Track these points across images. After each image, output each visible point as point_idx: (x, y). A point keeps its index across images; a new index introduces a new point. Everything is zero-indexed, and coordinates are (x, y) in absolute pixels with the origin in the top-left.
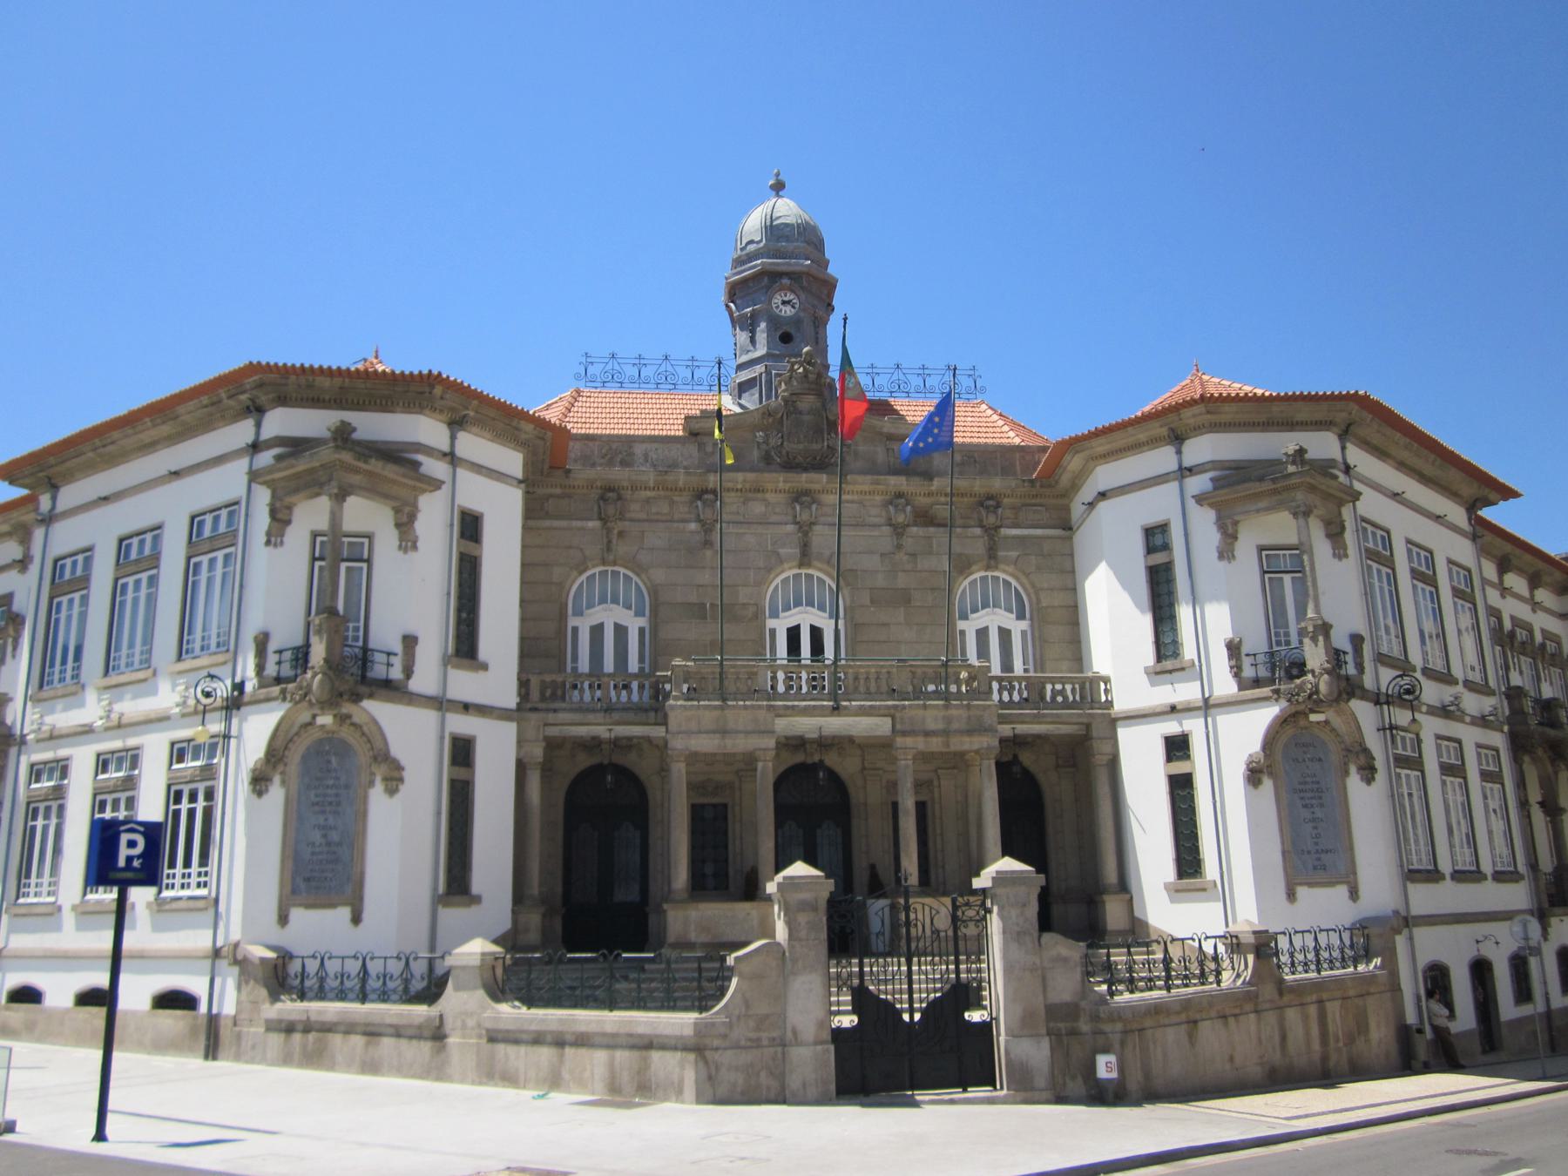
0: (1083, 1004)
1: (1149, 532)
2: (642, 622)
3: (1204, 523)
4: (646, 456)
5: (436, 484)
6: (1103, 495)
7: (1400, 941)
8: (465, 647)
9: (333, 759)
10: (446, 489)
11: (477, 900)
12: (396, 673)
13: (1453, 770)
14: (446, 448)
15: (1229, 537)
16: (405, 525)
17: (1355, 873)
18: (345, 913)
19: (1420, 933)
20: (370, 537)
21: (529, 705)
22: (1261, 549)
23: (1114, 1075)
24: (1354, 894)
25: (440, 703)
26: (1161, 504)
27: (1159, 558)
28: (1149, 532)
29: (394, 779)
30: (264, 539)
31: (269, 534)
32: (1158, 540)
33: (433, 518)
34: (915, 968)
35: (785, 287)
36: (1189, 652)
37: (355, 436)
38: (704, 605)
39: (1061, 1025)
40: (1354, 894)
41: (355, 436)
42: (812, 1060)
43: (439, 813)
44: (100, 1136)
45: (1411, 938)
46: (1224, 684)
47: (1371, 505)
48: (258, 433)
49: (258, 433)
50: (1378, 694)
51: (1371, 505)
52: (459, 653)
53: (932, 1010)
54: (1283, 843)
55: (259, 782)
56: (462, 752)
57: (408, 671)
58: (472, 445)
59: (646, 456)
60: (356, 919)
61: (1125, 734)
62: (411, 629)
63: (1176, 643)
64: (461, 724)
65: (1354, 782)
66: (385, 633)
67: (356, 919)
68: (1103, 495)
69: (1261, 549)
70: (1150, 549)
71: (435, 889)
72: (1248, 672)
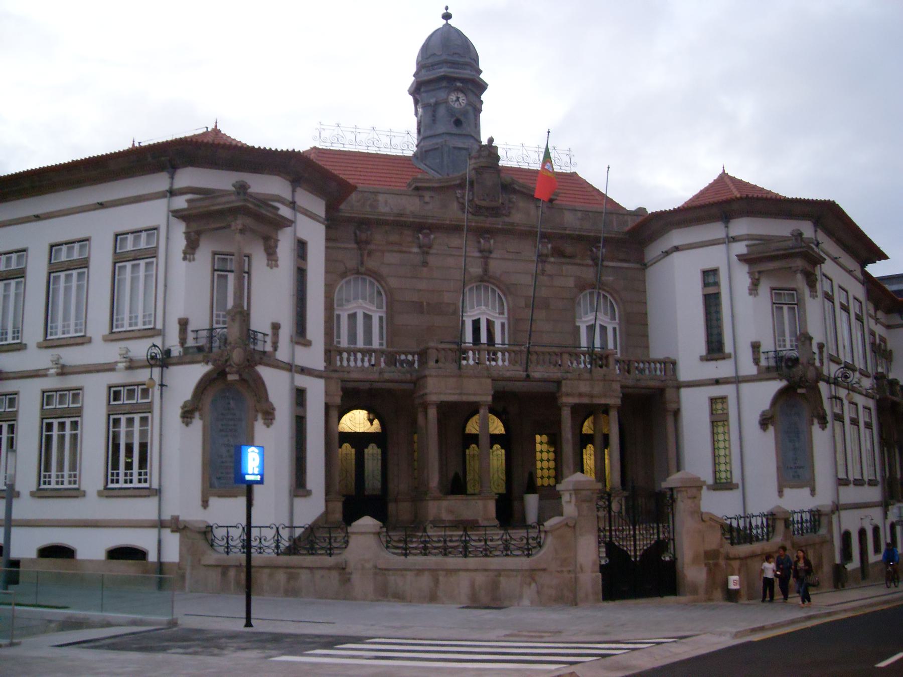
0: (721, 550)
1: (706, 273)
3: (179, 230)
4: (386, 202)
6: (677, 249)
7: (835, 518)
9: (231, 402)
12: (268, 348)
13: (854, 422)
17: (814, 480)
19: (844, 514)
21: (332, 368)
22: (773, 289)
23: (737, 587)
24: (813, 492)
25: (290, 367)
27: (711, 290)
28: (706, 273)
29: (269, 415)
30: (182, 255)
31: (185, 253)
32: (711, 279)
34: (637, 532)
35: (449, 76)
36: (728, 348)
37: (250, 190)
38: (422, 303)
39: (711, 562)
40: (813, 492)
41: (250, 190)
42: (590, 578)
44: (249, 624)
45: (839, 517)
48: (172, 184)
49: (172, 184)
50: (829, 378)
53: (646, 554)
54: (777, 462)
55: (187, 415)
56: (300, 395)
59: (386, 202)
61: (685, 393)
64: (302, 381)
65: (816, 428)
66: (260, 322)
68: (677, 249)
70: (706, 285)
72: (763, 363)
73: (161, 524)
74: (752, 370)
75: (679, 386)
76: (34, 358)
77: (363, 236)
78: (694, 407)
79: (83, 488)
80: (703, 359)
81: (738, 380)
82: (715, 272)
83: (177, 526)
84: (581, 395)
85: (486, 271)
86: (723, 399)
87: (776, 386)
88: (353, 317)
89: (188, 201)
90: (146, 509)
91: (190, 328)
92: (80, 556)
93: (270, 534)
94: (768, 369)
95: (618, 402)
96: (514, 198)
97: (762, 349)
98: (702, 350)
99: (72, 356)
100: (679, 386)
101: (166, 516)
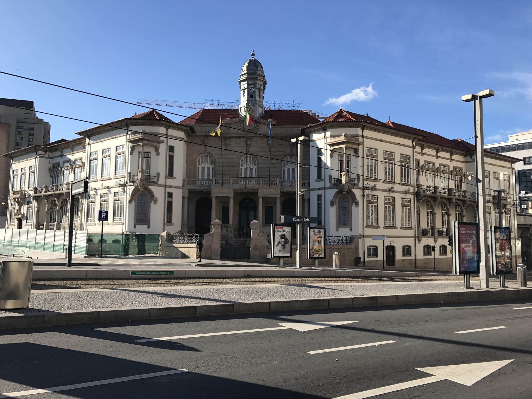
2: (213, 167)
5: (163, 142)
8: (171, 174)
10: (165, 142)
11: (173, 224)
12: (156, 180)
14: (166, 133)
16: (157, 150)
18: (146, 226)
20: (150, 152)
24: (351, 230)
25: (165, 186)
29: (357, 204)
33: (163, 148)
36: (323, 177)
40: (351, 230)
43: (165, 208)
46: (328, 185)
47: (368, 143)
51: (368, 143)
52: (169, 175)
56: (170, 195)
57: (158, 180)
58: (171, 132)
60: (149, 227)
62: (159, 171)
63: (321, 175)
67: (149, 227)
71: (164, 222)
72: (333, 182)
77: (249, 142)
80: (315, 180)
87: (335, 191)
88: (203, 168)
91: (333, 178)
93: (332, 238)
94: (334, 184)
95: (279, 196)
98: (316, 178)
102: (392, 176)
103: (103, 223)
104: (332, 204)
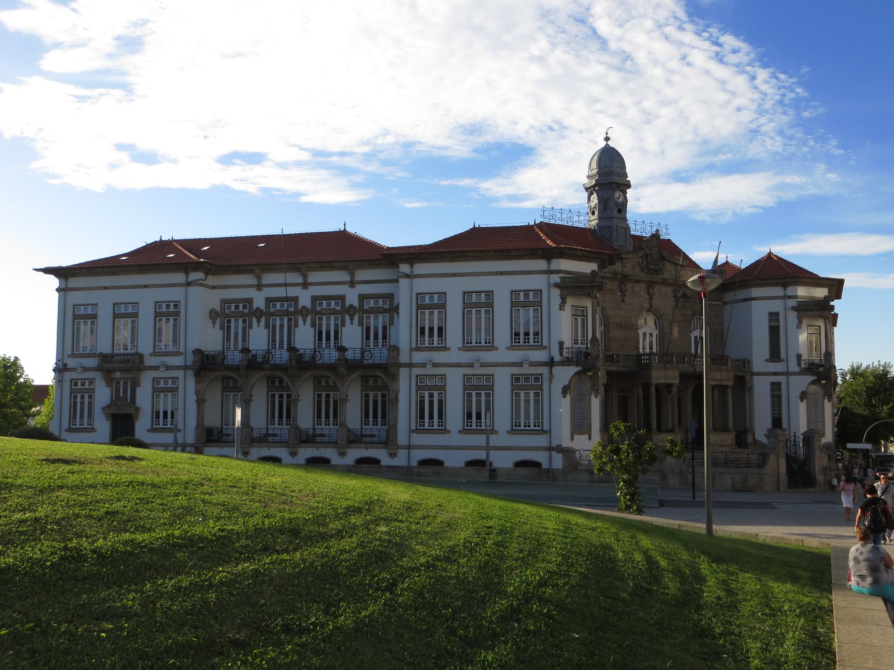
1: (771, 314)
3: (556, 293)
15: (564, 302)
18: (587, 436)
22: (573, 306)
26: (776, 306)
36: (783, 356)
44: (694, 498)
46: (794, 367)
60: (590, 438)
61: (756, 379)
67: (590, 438)
69: (573, 306)
70: (771, 320)
72: (803, 366)
73: (550, 449)
74: (797, 369)
75: (753, 374)
76: (454, 355)
78: (761, 389)
79: (448, 428)
80: (767, 361)
81: (787, 374)
82: (777, 314)
83: (560, 449)
84: (716, 380)
85: (651, 305)
86: (779, 384)
89: (561, 278)
90: (540, 441)
92: (446, 465)
94: (805, 369)
95: (677, 382)
96: (666, 264)
97: (803, 358)
99: (487, 356)
100: (753, 374)
101: (554, 445)
102: (75, 403)
103: (405, 365)
104: (565, 391)
